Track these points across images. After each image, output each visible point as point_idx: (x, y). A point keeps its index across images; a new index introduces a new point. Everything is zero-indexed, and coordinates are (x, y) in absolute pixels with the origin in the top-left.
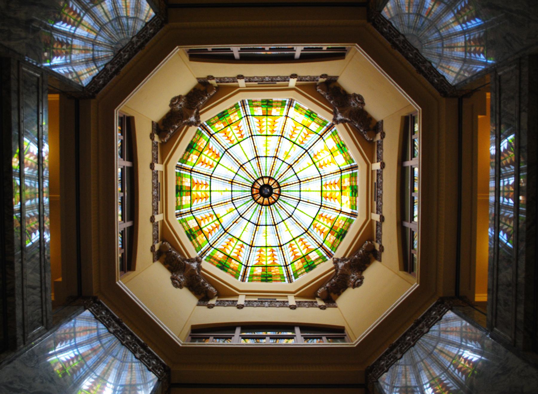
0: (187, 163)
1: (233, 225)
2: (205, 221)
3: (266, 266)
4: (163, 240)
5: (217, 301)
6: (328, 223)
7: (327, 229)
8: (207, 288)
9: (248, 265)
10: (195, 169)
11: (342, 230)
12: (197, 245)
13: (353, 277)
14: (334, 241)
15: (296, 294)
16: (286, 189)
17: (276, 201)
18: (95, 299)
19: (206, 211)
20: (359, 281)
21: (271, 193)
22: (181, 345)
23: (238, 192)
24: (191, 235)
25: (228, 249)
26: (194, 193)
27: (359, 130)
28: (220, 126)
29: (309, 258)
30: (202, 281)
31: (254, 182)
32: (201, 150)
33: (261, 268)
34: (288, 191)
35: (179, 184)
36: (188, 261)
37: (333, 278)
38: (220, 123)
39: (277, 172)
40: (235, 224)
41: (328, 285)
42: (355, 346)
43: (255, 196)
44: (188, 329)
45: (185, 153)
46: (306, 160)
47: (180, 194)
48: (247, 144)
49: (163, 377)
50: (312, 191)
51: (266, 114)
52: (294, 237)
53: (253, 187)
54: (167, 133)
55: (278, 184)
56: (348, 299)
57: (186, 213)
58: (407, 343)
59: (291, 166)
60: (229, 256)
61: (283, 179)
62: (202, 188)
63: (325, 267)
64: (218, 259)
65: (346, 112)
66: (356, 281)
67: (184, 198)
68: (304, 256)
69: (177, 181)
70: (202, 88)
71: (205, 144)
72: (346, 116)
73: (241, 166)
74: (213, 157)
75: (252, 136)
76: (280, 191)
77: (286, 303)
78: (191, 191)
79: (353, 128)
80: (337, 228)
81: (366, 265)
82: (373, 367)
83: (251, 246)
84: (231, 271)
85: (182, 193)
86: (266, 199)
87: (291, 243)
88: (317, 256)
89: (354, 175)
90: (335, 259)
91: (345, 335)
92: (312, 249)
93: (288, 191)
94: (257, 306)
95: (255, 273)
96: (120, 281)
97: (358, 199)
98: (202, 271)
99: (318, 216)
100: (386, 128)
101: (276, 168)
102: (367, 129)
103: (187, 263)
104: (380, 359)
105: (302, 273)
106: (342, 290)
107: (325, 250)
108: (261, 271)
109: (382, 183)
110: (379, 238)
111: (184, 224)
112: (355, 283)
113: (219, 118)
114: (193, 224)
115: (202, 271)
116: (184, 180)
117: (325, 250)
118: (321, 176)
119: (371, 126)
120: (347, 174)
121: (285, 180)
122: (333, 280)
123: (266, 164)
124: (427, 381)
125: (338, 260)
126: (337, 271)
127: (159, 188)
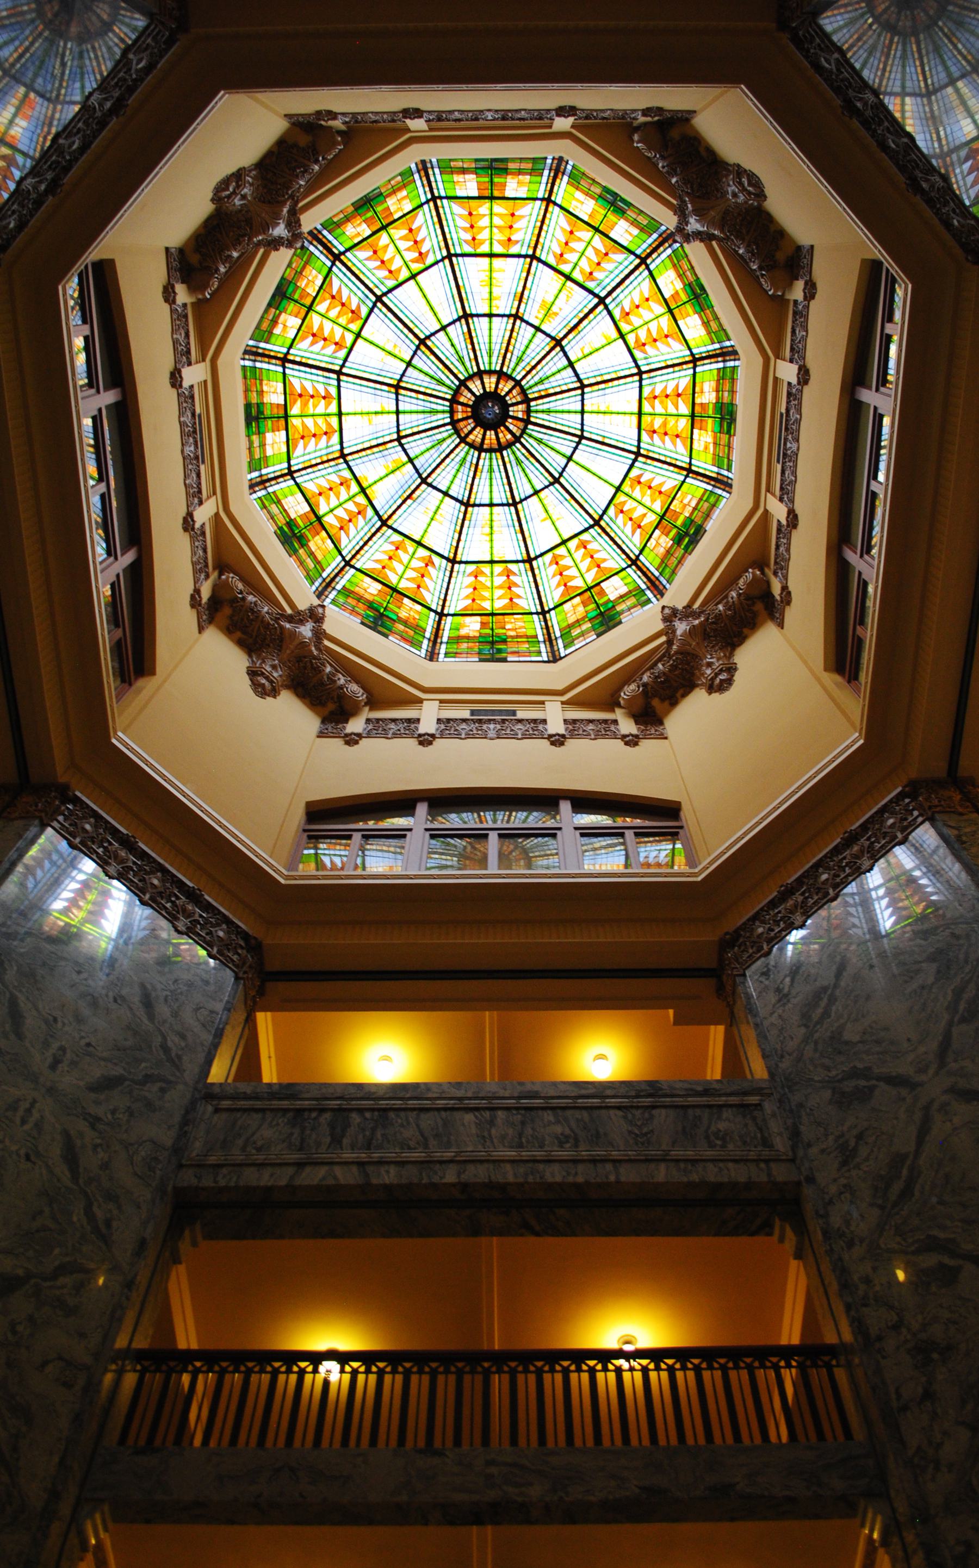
0: (273, 340)
1: (404, 506)
2: (328, 498)
3: (493, 614)
4: (222, 567)
5: (368, 721)
6: (653, 501)
7: (652, 518)
8: (341, 687)
9: (446, 612)
10: (295, 354)
11: (690, 521)
12: (310, 564)
13: (709, 665)
14: (668, 552)
15: (565, 698)
16: (545, 407)
17: (517, 439)
18: (65, 794)
19: (330, 470)
20: (723, 676)
21: (505, 415)
22: (282, 881)
23: (415, 416)
24: (292, 537)
25: (393, 570)
26: (295, 422)
27: (747, 263)
28: (359, 229)
29: (602, 593)
30: (328, 669)
31: (458, 387)
32: (308, 302)
33: (478, 618)
34: (548, 412)
35: (254, 399)
36: (290, 619)
37: (660, 660)
40: (409, 502)
41: (645, 678)
42: (699, 879)
43: (462, 424)
44: (298, 814)
45: (266, 311)
46: (601, 326)
47: (258, 427)
48: (436, 281)
49: (245, 969)
50: (613, 413)
51: (487, 193)
52: (565, 537)
53: (454, 401)
54: (211, 276)
55: (523, 392)
56: (694, 714)
57: (276, 478)
58: (819, 889)
59: (558, 343)
60: (394, 590)
61: (536, 379)
62: (315, 406)
63: (641, 625)
64: (367, 596)
65: (712, 213)
66: (717, 675)
67: (269, 437)
68: (589, 589)
69: (246, 391)
70: (304, 140)
71: (319, 282)
72: (711, 223)
74: (343, 321)
75: (450, 256)
76: (528, 411)
77: (541, 727)
78: (286, 417)
79: (732, 256)
80: (677, 515)
81: (745, 631)
82: (737, 933)
83: (453, 561)
84: (400, 627)
85: (262, 424)
86: (491, 434)
87: (557, 551)
88: (624, 590)
89: (728, 375)
90: (667, 611)
91: (681, 827)
92: (611, 569)
93: (548, 412)
94: (469, 736)
95: (463, 632)
96: (120, 734)
97: (736, 441)
98: (326, 643)
99: (627, 481)
100: (821, 269)
102: (769, 265)
103: (288, 626)
104: (755, 918)
105: (583, 634)
106: (681, 691)
107: (644, 572)
108: (478, 626)
109: (798, 422)
110: (782, 566)
111: (274, 509)
112: (713, 679)
113: (356, 209)
114: (297, 507)
116: (265, 388)
117: (644, 572)
118: (640, 373)
119: (780, 256)
120: (708, 371)
121: (541, 382)
122: (660, 666)
123: (490, 335)
124: (881, 881)
125: (674, 611)
126: (670, 642)
127: (200, 436)
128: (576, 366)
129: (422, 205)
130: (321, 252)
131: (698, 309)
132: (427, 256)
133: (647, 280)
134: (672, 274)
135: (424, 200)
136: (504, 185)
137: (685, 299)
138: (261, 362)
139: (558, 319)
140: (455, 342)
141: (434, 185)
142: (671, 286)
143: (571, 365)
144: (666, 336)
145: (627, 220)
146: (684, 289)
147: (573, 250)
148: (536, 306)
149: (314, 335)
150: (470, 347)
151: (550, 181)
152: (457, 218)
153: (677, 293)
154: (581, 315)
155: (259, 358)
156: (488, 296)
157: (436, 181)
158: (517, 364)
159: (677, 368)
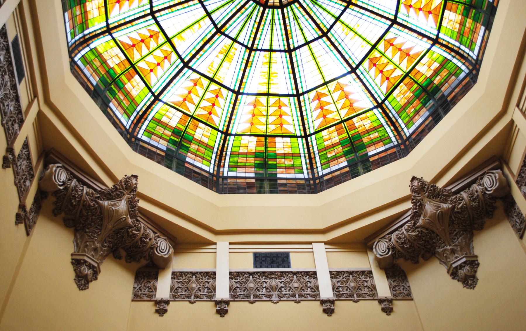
0: (441, 59)
10: (426, 44)
32: (407, 80)
38: (360, 130)
39: (249, 16)
71: (396, 92)
73: (325, 35)
75: (298, 95)
90: (134, 181)
101: (251, 25)
115: (440, 185)
116: (457, 26)
128: (204, 14)
129: (315, 133)
130: (390, 111)
131: (112, 72)
132: (315, 97)
133: (153, 84)
134: (134, 93)
135: (313, 136)
136: (257, 145)
137: (123, 77)
138: (454, 45)
139: (219, 49)
140: (299, 32)
141: (305, 146)
142: (134, 84)
143: (209, 14)
144: (134, 46)
145: (171, 127)
146: (124, 84)
147: (208, 100)
148: (236, 58)
149: (408, 55)
150: (288, 28)
151: (225, 148)
152: (292, 123)
153: (129, 80)
154: (201, 53)
155: (455, 48)
156: (272, 65)
157: (304, 148)
158: (252, 13)
159: (123, 22)
